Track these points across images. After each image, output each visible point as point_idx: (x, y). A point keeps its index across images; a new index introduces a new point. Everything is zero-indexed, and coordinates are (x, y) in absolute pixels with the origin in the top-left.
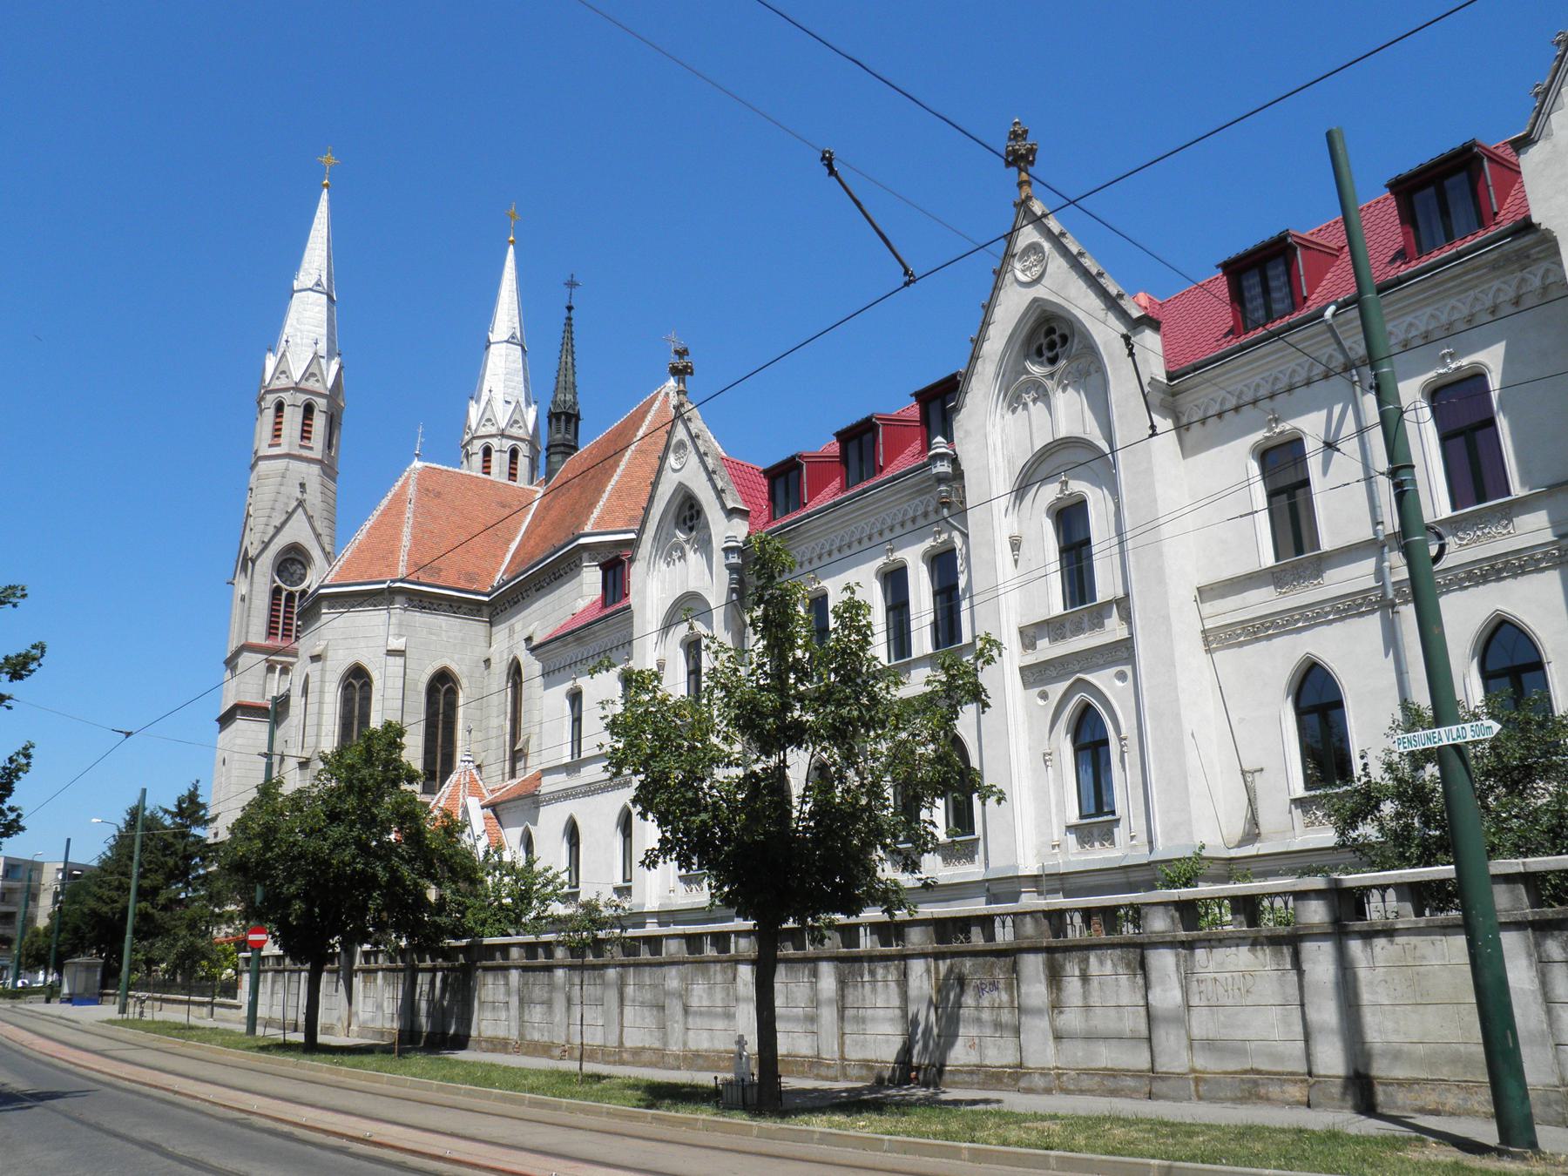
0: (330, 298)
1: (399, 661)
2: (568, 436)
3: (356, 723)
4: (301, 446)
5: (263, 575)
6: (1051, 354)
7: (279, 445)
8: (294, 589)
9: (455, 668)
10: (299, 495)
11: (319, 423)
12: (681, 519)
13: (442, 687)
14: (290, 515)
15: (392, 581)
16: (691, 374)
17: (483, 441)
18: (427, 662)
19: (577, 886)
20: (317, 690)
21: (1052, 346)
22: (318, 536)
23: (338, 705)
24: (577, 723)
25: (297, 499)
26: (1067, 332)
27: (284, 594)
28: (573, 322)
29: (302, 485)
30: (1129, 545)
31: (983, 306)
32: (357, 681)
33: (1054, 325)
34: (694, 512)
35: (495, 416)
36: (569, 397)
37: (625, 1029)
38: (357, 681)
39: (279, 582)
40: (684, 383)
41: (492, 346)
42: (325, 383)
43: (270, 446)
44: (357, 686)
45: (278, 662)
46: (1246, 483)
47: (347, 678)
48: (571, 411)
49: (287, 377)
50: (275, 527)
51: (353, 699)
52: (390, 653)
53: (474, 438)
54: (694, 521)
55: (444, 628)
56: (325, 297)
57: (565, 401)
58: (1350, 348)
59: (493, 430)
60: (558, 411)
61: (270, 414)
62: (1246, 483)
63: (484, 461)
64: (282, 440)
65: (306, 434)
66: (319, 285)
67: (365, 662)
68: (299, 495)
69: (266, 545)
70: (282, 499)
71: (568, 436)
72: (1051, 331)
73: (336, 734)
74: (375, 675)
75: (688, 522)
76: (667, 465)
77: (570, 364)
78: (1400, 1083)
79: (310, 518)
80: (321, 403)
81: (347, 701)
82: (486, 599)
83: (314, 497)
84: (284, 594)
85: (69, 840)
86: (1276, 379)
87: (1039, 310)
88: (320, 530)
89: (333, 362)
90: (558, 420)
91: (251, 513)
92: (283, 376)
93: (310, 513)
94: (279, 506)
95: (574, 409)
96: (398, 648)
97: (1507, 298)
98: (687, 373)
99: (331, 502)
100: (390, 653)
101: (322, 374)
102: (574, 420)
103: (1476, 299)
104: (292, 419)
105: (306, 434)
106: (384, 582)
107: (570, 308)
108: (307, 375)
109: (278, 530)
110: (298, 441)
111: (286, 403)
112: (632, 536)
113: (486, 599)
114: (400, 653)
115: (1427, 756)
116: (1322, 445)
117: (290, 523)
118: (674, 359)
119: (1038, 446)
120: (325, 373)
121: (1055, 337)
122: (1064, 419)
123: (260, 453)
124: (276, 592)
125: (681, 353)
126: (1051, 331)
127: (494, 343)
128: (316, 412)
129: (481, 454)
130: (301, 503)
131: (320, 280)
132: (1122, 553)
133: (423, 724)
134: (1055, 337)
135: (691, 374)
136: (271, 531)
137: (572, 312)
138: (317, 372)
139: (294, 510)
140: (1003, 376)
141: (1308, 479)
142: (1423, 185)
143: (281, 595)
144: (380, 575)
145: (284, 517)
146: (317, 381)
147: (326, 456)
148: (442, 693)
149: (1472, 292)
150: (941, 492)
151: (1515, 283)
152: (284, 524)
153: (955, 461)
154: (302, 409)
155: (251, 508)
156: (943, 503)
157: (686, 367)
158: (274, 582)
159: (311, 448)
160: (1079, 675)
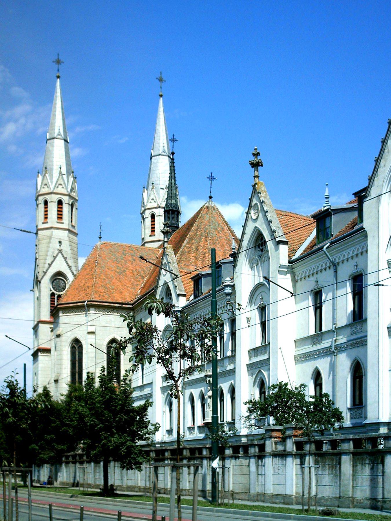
0: (66, 141)
2: (173, 222)
3: (77, 363)
4: (58, 222)
5: (46, 287)
7: (47, 223)
8: (60, 293)
10: (58, 247)
11: (66, 209)
14: (55, 258)
15: (88, 301)
16: (262, 166)
17: (150, 211)
18: (106, 336)
19: (223, 421)
22: (70, 267)
24: (318, 310)
25: (58, 250)
27: (56, 296)
28: (174, 161)
29: (60, 242)
30: (144, 376)
31: (243, 226)
34: (263, 241)
35: (155, 197)
36: (173, 201)
37: (302, 484)
39: (53, 291)
40: (258, 171)
41: (153, 158)
42: (67, 189)
43: (43, 223)
44: (77, 348)
47: (72, 344)
48: (174, 209)
49: (48, 187)
50: (49, 264)
51: (75, 353)
52: (89, 333)
53: (145, 209)
54: (263, 247)
56: (63, 141)
57: (171, 204)
59: (155, 205)
60: (168, 209)
61: (42, 206)
63: (152, 221)
64: (48, 220)
65: (60, 216)
66: (59, 135)
68: (58, 247)
69: (45, 273)
70: (51, 250)
71: (173, 222)
74: (83, 343)
75: (260, 247)
76: (250, 217)
77: (173, 184)
78: (21, 512)
79: (65, 259)
80: (66, 200)
81: (73, 354)
82: (131, 306)
83: (66, 247)
84: (56, 296)
87: (257, 231)
88: (70, 265)
89: (70, 176)
90: (168, 213)
91: (37, 257)
92: (45, 187)
93: (65, 256)
94: (50, 253)
95: (176, 208)
96: (93, 331)
98: (260, 166)
99: (75, 249)
100: (89, 333)
101: (65, 184)
102: (176, 213)
104: (53, 208)
105: (60, 216)
108: (57, 185)
109: (50, 265)
110: (56, 220)
111: (49, 201)
113: (131, 306)
114: (93, 333)
117: (55, 261)
118: (253, 159)
119: (256, 284)
120: (67, 185)
123: (39, 227)
124: (53, 295)
125: (256, 155)
127: (154, 156)
128: (64, 204)
129: (150, 218)
130: (60, 251)
131: (59, 132)
132: (143, 378)
135: (262, 166)
136: (47, 266)
137: (174, 155)
138: (62, 183)
139: (57, 255)
140: (248, 255)
143: (55, 296)
145: (52, 259)
146: (63, 188)
147: (71, 226)
150: (227, 299)
152: (52, 262)
153: (233, 287)
154: (56, 203)
155: (37, 255)
156: (228, 304)
157: (258, 163)
158: (51, 291)
159: (63, 223)
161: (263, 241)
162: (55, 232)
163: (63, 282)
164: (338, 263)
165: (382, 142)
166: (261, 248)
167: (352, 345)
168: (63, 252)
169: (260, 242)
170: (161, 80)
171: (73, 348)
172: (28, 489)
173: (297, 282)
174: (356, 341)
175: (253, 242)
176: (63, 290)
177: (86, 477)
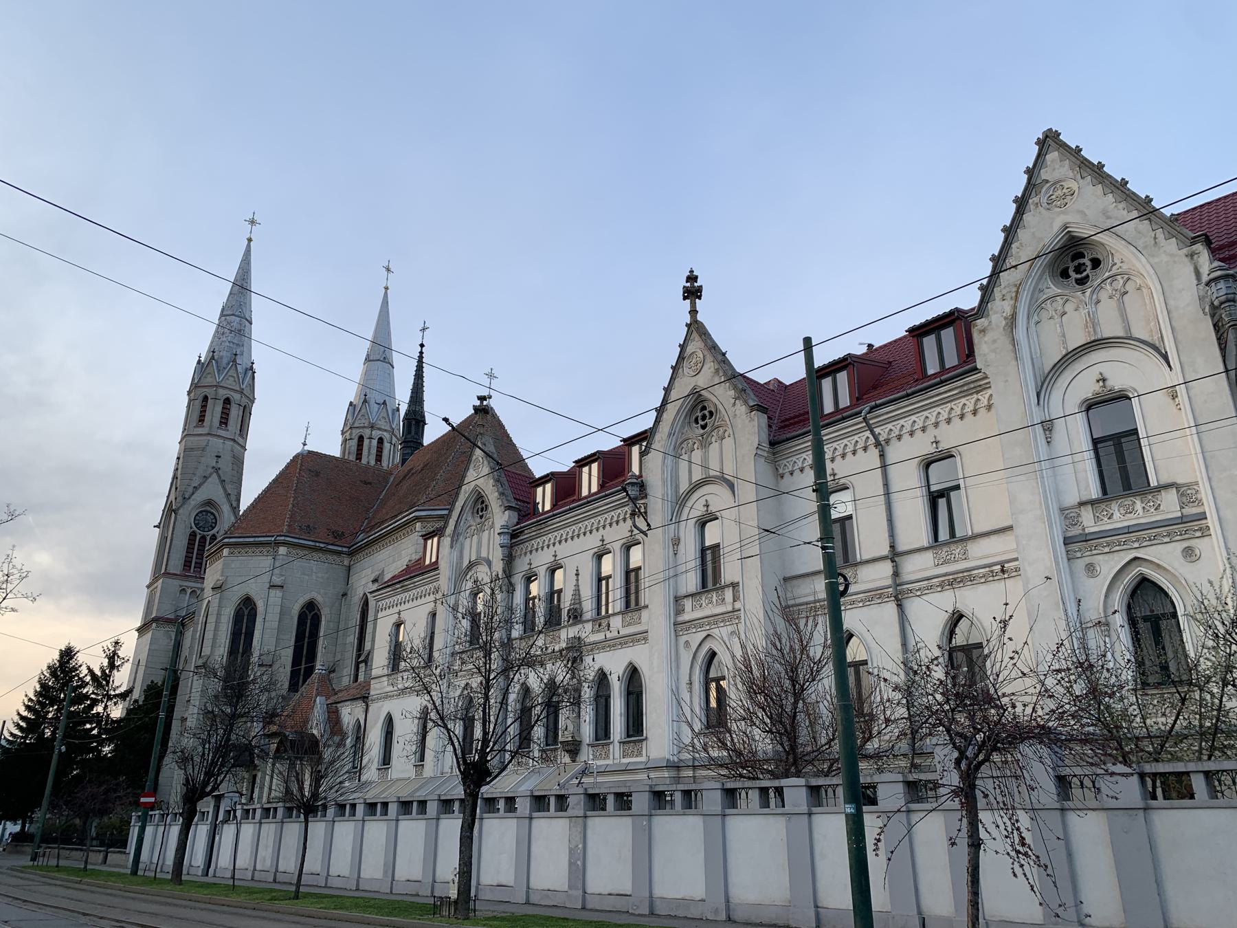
1: (278, 593)
6: (703, 423)
9: (319, 599)
12: (475, 511)
13: (309, 618)
17: (358, 431)
20: (215, 612)
21: (704, 418)
23: (230, 624)
26: (713, 410)
32: (246, 613)
33: (706, 404)
38: (246, 613)
44: (246, 613)
45: (188, 587)
46: (743, 543)
55: (314, 570)
58: (879, 434)
62: (743, 543)
67: (253, 595)
72: (704, 408)
73: (227, 646)
85: (4, 722)
86: (836, 449)
97: (919, 427)
103: (952, 409)
106: (273, 536)
107: (422, 346)
112: (446, 512)
115: (71, 723)
116: (756, 531)
121: (706, 412)
122: (46, 795)
126: (704, 408)
128: (233, 404)
130: (217, 470)
133: (292, 648)
134: (706, 412)
137: (424, 348)
141: (1136, 429)
142: (927, 333)
144: (269, 531)
148: (309, 618)
149: (949, 404)
151: (973, 401)
152: (200, 485)
160: (1140, 568)
161: (484, 505)
162: (213, 440)
163: (212, 517)
164: (887, 441)
165: (1124, 183)
166: (481, 514)
167: (941, 585)
168: (220, 472)
169: (480, 506)
170: (388, 270)
171: (238, 617)
172: (202, 876)
173: (782, 477)
174: (956, 576)
175: (687, 410)
176: (210, 528)
177: (1170, 654)
